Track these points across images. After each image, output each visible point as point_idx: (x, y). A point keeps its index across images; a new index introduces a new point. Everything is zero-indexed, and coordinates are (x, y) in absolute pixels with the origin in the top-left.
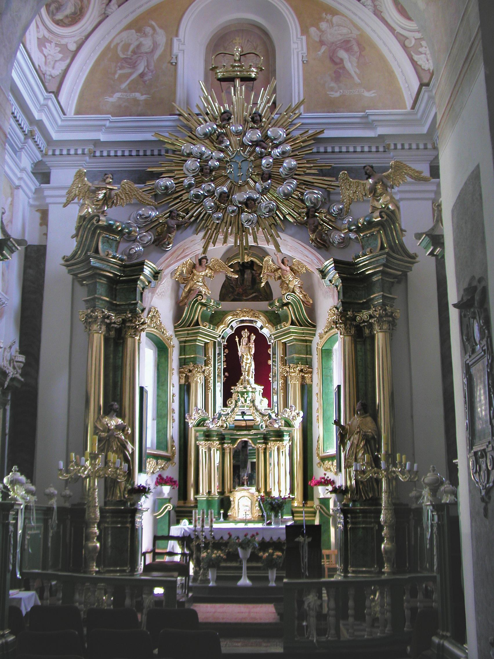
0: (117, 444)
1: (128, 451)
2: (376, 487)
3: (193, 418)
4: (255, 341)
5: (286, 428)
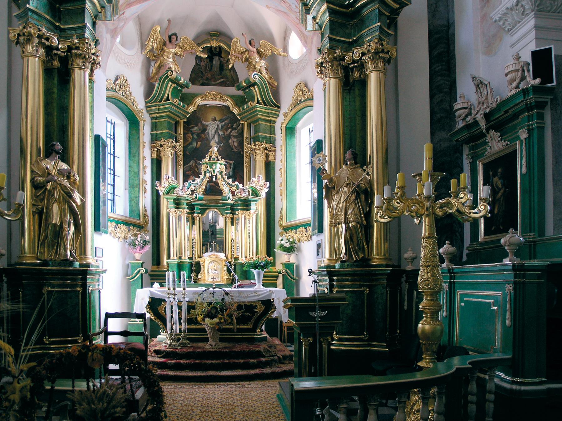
0: (60, 192)
1: (75, 202)
2: (366, 247)
3: (163, 186)
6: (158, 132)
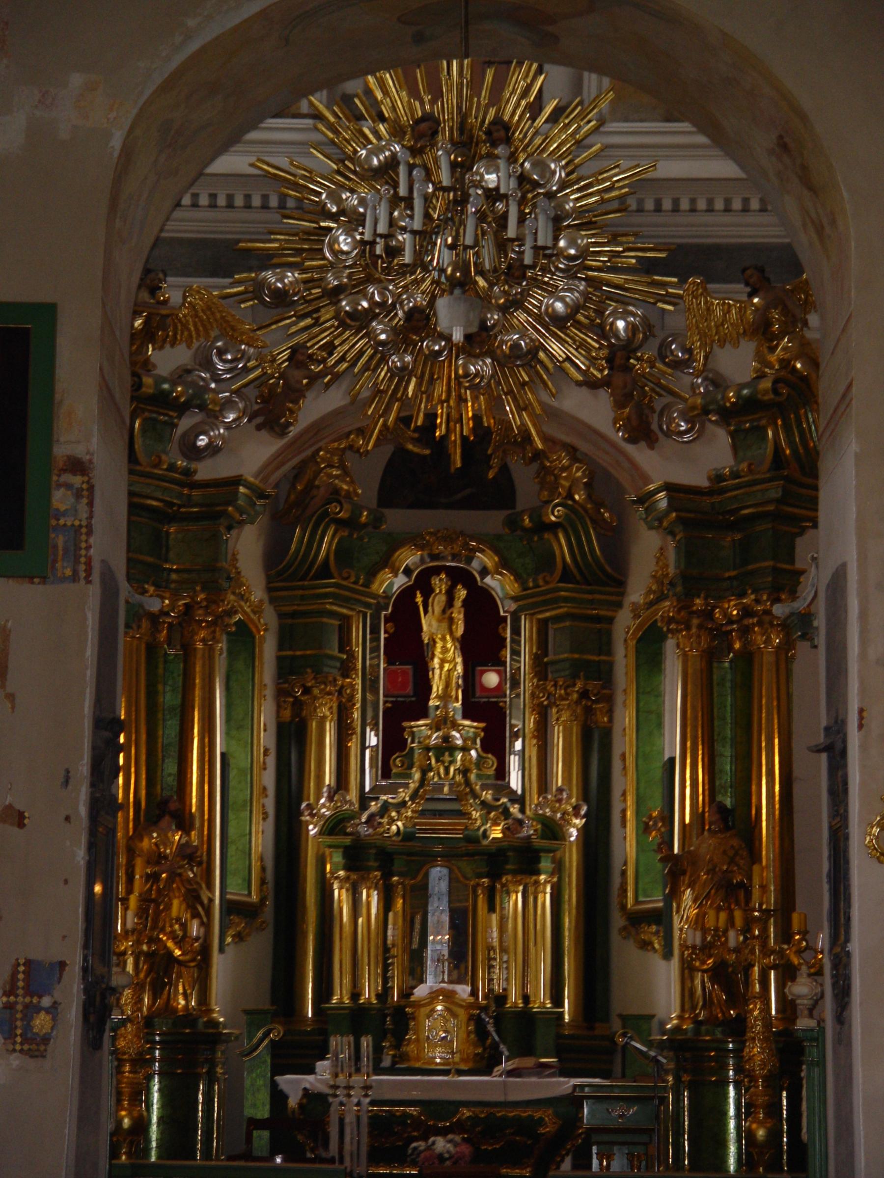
4: (465, 603)
5: (545, 843)
6: (298, 653)
